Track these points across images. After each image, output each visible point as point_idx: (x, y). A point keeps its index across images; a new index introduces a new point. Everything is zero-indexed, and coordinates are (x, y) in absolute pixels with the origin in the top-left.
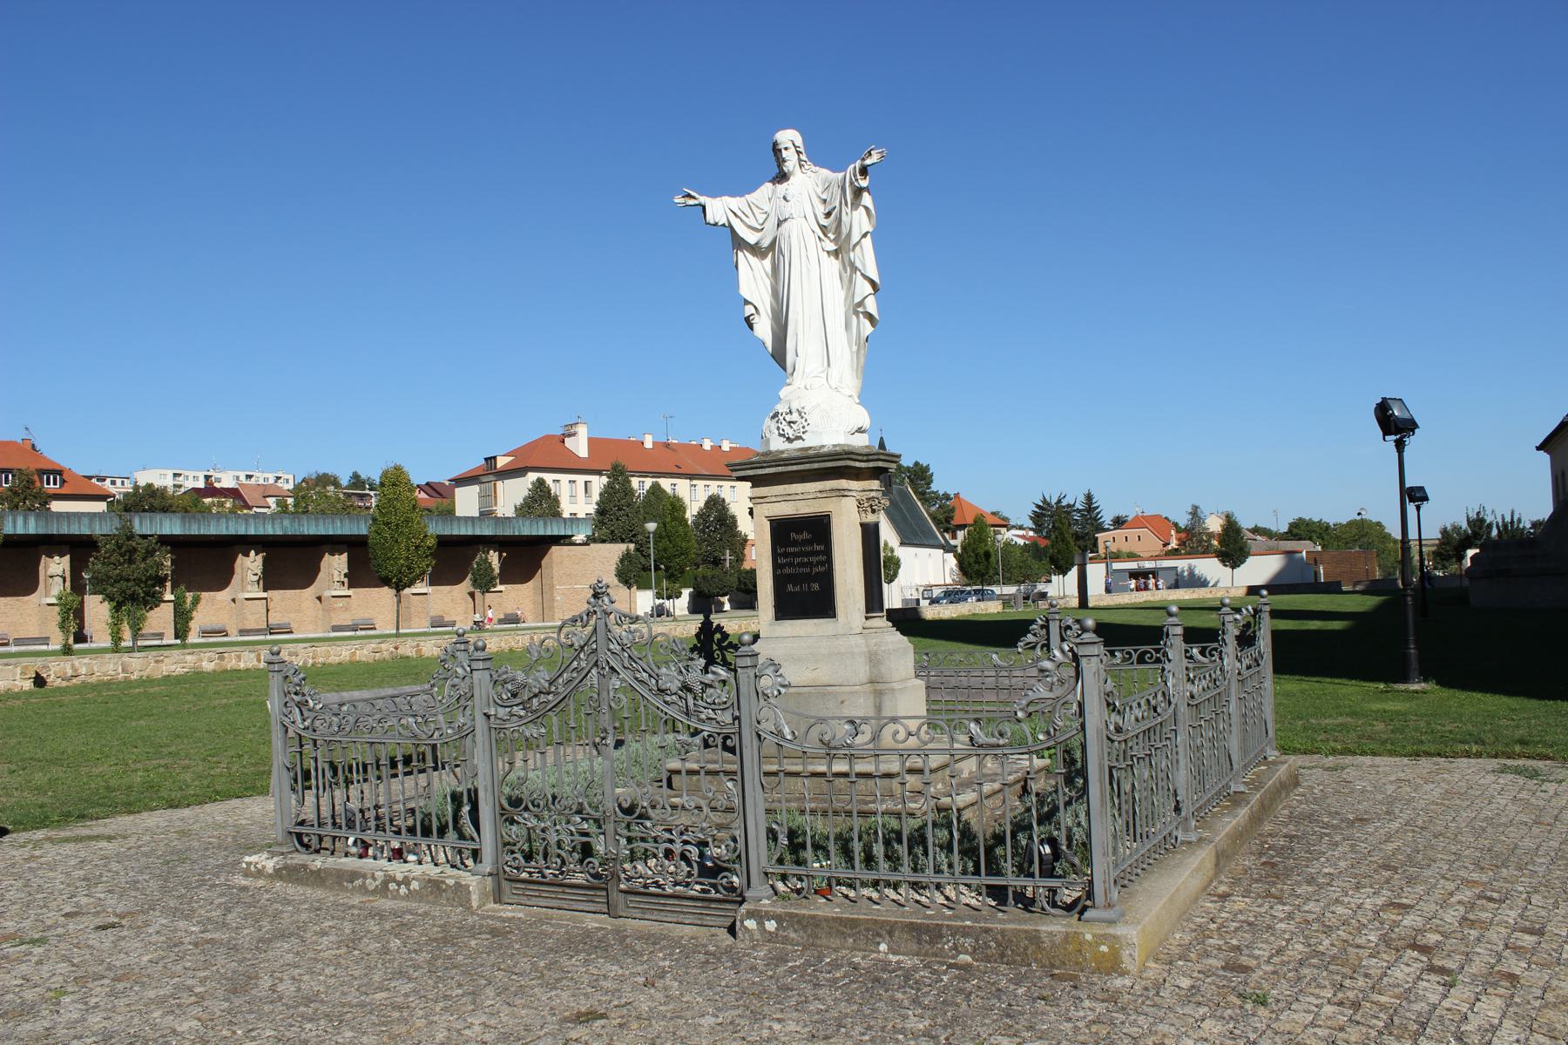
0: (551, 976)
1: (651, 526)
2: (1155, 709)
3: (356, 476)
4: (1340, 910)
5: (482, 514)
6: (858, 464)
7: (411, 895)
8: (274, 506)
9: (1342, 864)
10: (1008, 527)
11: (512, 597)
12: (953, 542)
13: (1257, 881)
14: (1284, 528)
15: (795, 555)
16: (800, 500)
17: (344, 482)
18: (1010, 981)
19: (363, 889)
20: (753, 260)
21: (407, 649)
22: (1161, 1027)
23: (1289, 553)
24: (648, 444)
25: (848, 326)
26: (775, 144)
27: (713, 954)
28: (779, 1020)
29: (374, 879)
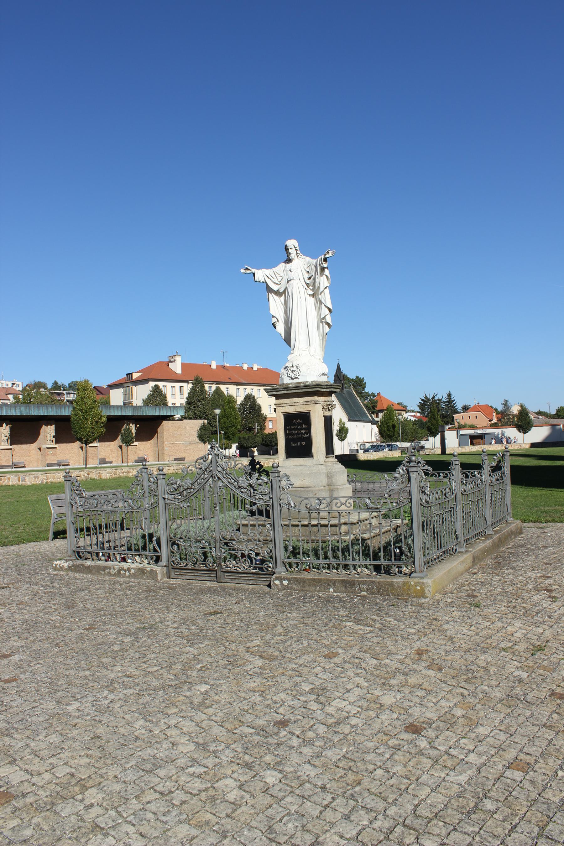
0: (197, 601)
1: (218, 411)
2: (445, 495)
3: (55, 383)
4: (521, 578)
5: (124, 404)
6: (322, 390)
7: (131, 576)
8: (12, 399)
9: (529, 563)
10: (406, 411)
11: (143, 448)
12: (376, 419)
13: (490, 568)
14: (554, 412)
15: (295, 429)
16: (297, 405)
17: (49, 386)
18: (381, 600)
19: (109, 574)
20: (276, 297)
21: (94, 475)
22: (436, 614)
23: (553, 426)
24: (214, 366)
25: (318, 327)
26: (286, 246)
27: (262, 594)
28: (289, 613)
29: (114, 569)
